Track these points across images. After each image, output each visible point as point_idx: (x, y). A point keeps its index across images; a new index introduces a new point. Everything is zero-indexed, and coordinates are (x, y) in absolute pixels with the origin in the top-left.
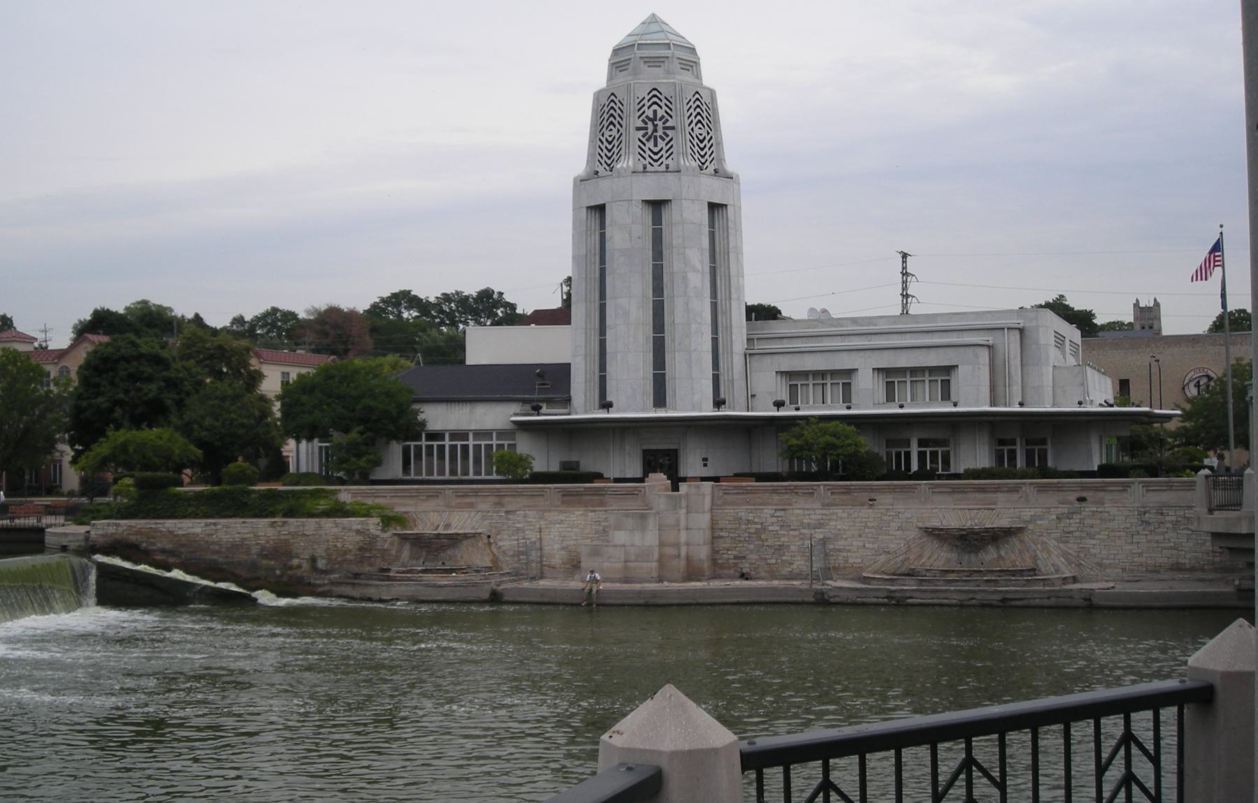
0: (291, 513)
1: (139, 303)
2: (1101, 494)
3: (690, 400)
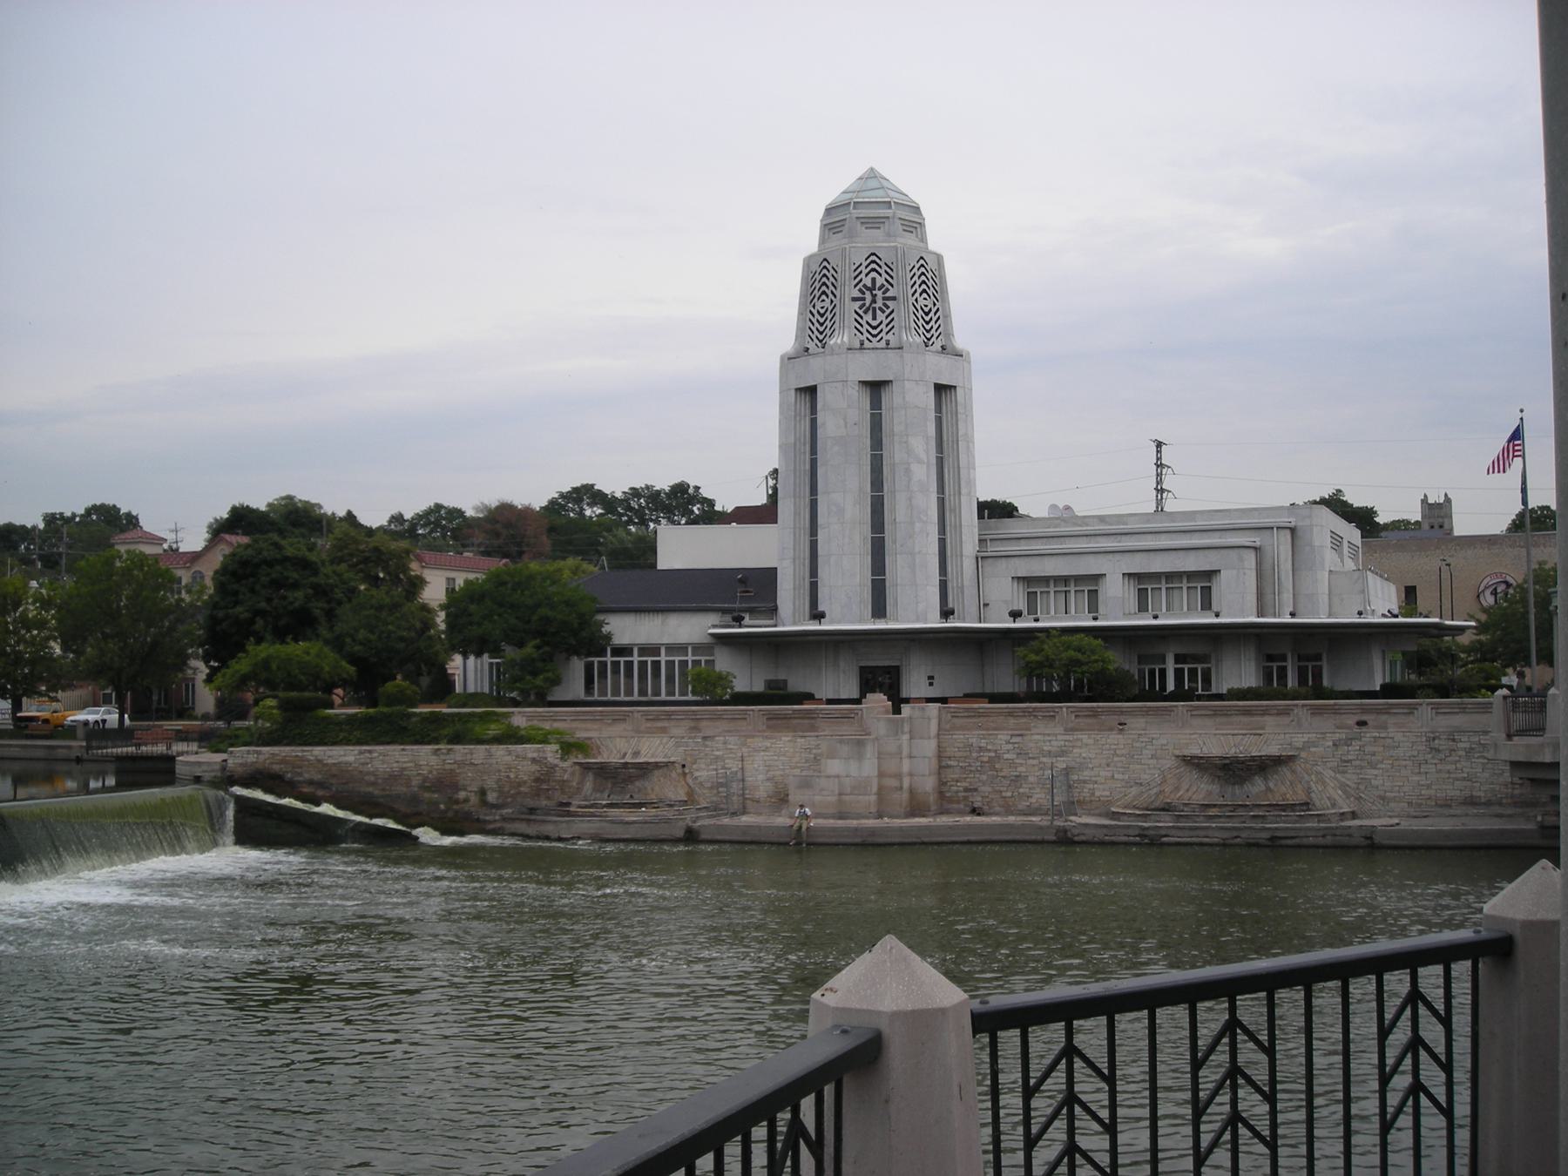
0: (457, 739)
2: (1384, 717)
3: (917, 610)
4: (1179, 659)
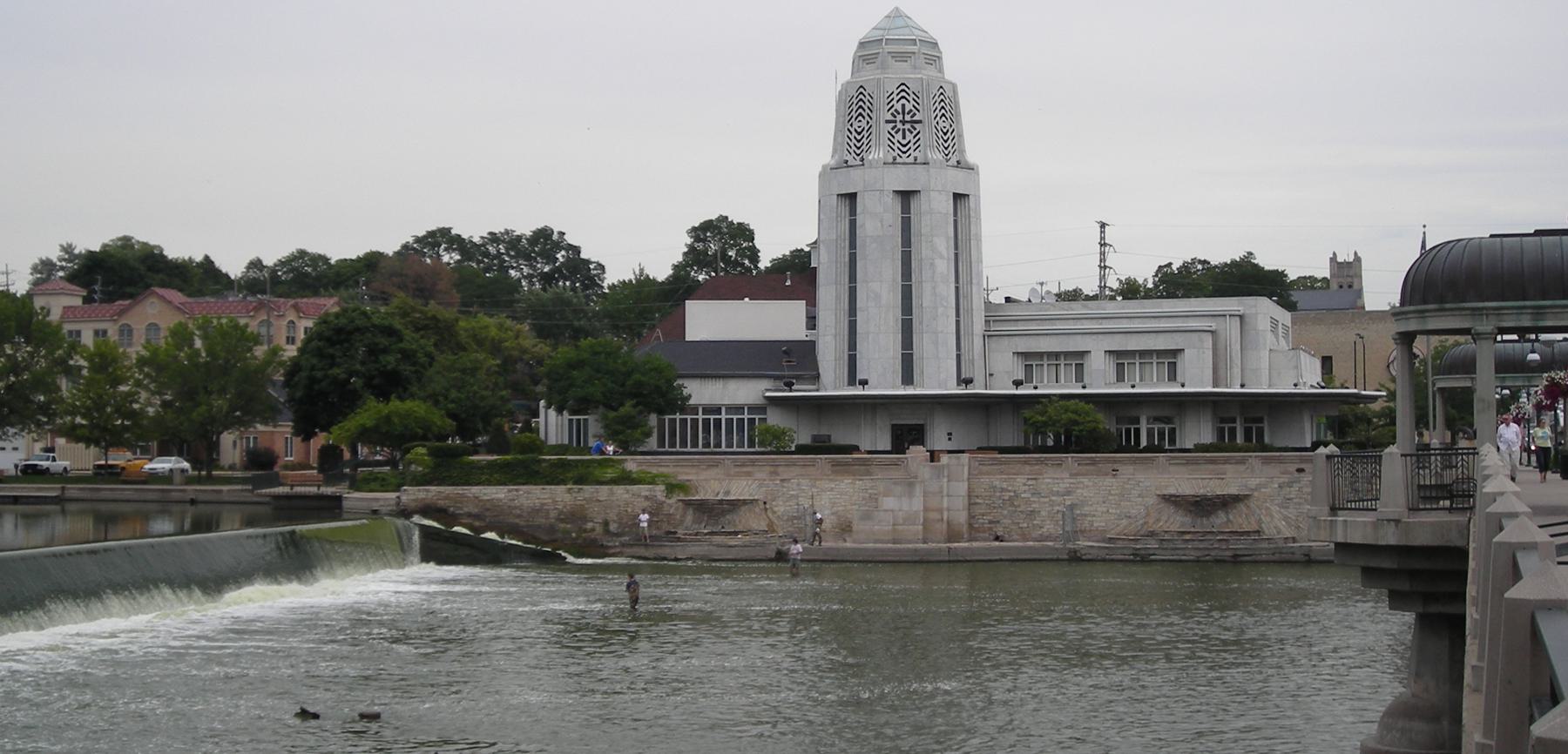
0: (581, 481)
1: (119, 239)
3: (937, 380)
4: (1246, 420)
